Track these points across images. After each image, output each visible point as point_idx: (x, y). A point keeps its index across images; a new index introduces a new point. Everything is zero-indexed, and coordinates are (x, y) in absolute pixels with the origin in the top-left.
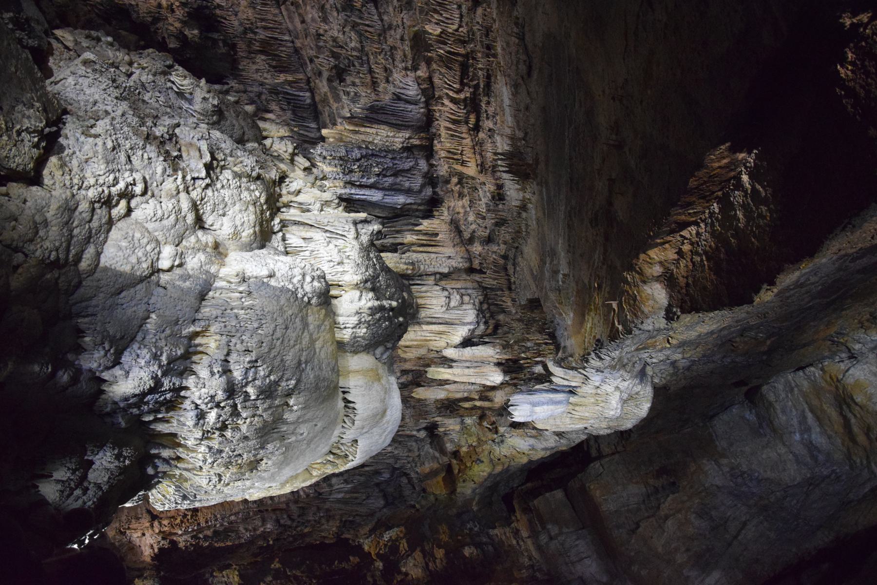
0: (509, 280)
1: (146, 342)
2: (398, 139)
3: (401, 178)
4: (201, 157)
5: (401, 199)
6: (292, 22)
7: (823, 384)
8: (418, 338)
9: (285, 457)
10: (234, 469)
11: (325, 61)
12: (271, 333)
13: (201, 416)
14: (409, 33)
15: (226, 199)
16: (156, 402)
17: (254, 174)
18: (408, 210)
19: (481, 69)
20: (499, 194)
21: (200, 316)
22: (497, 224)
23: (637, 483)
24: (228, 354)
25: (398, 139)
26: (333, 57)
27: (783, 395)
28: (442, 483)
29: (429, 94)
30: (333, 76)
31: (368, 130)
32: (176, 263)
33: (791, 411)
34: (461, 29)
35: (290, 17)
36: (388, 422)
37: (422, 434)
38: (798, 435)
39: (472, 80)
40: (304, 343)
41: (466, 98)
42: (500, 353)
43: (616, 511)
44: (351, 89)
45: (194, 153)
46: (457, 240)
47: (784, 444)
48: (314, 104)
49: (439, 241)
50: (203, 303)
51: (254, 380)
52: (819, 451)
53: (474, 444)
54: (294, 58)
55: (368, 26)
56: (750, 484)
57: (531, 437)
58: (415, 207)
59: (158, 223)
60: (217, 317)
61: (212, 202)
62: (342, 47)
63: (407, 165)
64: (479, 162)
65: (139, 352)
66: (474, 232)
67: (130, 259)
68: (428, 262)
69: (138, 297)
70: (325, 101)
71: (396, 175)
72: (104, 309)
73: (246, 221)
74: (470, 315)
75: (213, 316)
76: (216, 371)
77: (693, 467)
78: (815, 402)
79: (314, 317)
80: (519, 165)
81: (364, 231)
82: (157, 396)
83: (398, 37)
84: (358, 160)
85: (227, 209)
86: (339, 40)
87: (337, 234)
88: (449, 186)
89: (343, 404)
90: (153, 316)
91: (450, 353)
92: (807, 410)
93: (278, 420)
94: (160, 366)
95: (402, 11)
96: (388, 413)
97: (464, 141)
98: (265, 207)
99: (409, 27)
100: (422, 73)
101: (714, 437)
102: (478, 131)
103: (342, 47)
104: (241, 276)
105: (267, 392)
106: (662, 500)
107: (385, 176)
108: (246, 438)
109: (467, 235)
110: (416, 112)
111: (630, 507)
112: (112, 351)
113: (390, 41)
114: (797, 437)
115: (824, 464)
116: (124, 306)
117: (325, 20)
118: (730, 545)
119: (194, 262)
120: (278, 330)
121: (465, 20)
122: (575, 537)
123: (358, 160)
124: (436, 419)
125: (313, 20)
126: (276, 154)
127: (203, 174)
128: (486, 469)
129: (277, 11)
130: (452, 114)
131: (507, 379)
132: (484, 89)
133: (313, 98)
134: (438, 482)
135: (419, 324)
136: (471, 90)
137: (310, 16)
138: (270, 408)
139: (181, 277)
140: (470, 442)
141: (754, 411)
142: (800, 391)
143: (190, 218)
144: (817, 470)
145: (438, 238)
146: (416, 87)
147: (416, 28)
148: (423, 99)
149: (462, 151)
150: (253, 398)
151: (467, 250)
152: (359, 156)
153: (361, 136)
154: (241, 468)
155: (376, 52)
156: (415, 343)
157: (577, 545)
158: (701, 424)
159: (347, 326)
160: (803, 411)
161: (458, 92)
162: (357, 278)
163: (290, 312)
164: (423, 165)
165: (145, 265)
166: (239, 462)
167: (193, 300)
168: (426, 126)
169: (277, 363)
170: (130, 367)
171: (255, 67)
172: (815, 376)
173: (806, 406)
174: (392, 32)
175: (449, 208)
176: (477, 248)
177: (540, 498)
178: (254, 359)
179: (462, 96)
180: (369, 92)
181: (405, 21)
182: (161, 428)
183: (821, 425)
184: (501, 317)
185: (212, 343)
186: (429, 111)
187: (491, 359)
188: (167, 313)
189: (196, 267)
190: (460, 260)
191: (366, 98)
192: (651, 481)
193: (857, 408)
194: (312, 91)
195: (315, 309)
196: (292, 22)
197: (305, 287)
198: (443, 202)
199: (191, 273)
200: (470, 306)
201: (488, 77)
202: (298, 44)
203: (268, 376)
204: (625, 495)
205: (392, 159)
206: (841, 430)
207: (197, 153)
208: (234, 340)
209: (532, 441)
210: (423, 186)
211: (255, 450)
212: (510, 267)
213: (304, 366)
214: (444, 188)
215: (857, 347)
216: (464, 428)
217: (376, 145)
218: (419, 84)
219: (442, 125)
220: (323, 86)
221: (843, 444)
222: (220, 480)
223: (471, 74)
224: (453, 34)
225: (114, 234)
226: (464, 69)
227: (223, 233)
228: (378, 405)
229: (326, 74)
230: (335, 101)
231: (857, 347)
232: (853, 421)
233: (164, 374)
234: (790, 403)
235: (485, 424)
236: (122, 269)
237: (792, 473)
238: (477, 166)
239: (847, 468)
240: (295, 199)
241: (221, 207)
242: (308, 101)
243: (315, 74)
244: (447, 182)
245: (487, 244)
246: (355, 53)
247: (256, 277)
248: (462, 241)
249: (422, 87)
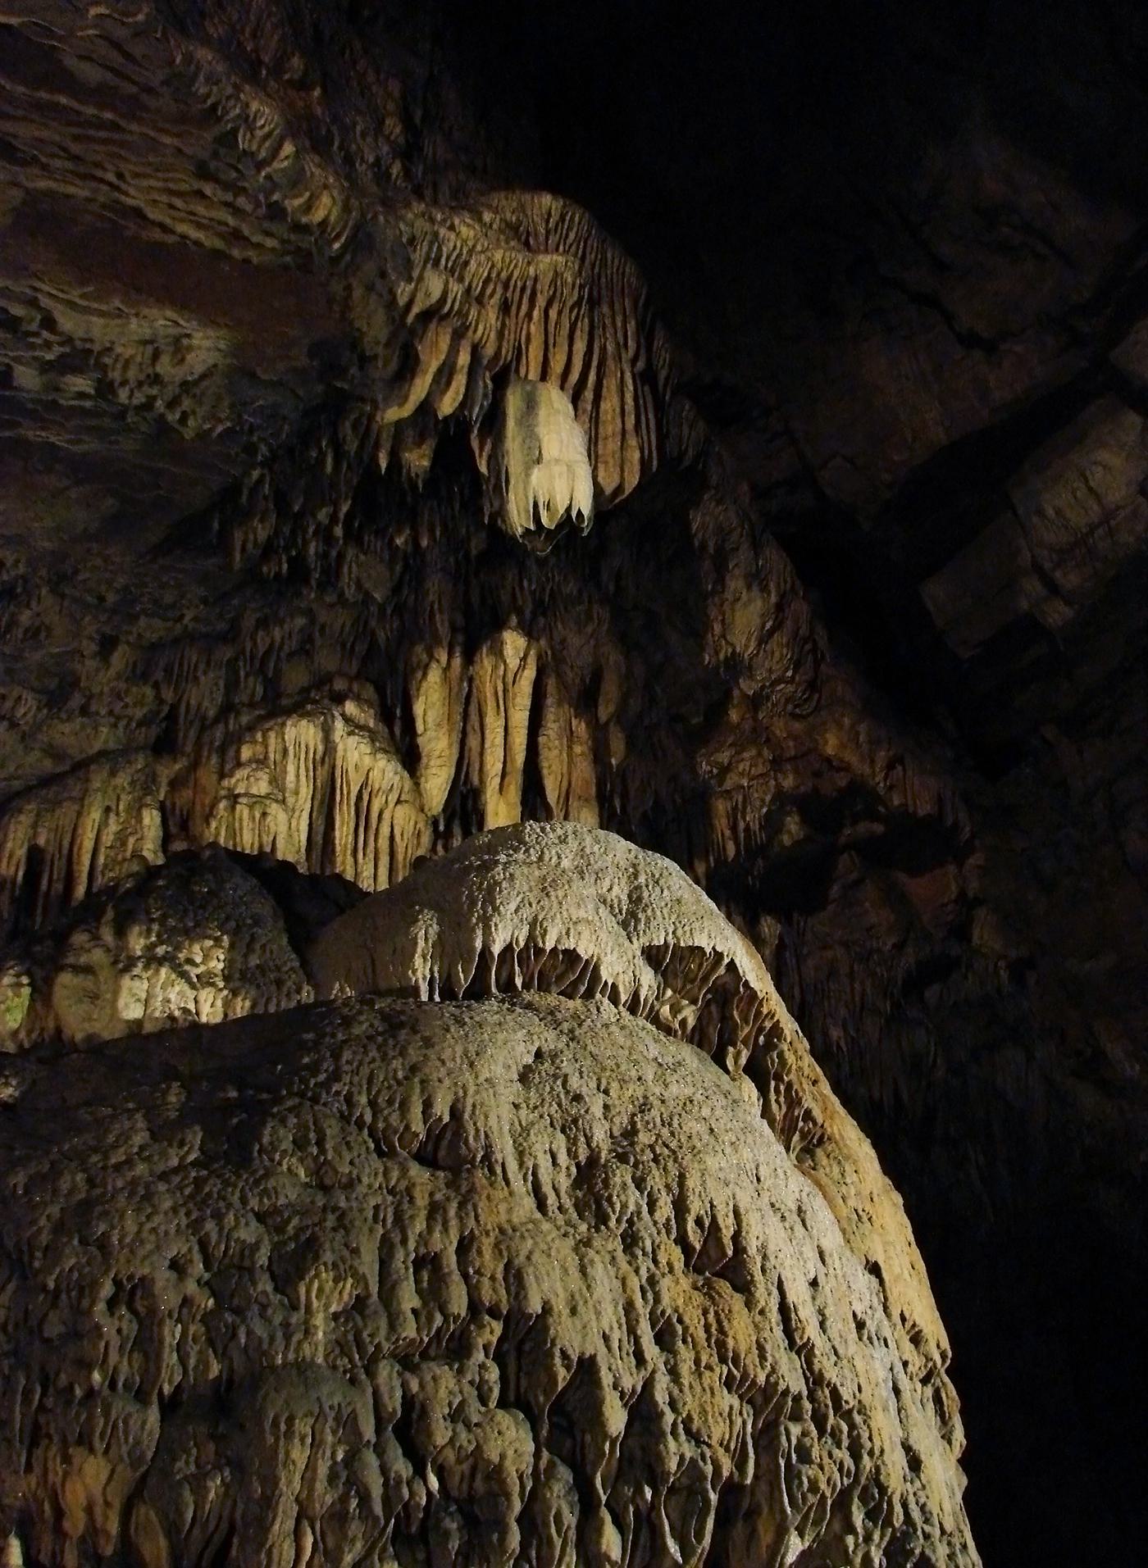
91: (437, 783)
131: (514, 620)
157: (1058, 512)
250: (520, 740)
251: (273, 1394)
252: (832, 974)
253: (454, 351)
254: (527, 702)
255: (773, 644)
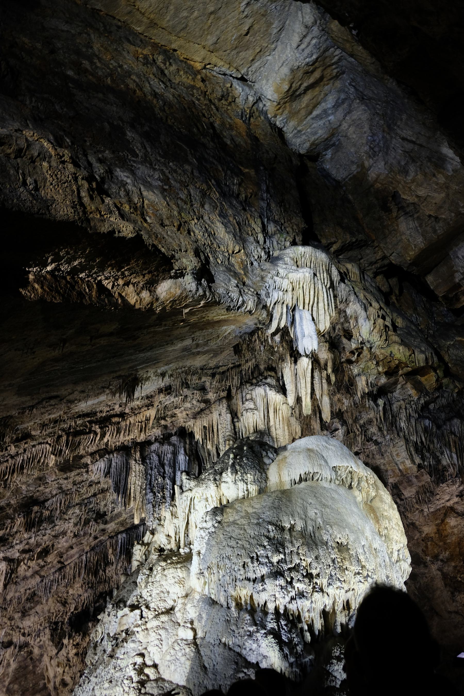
0: (232, 368)
1: (241, 644)
2: (137, 468)
3: (165, 461)
4: (126, 615)
5: (182, 458)
6: (74, 555)
7: (286, 112)
8: (281, 426)
9: (335, 524)
10: (347, 564)
11: (92, 528)
12: (232, 549)
13: (301, 595)
14: (61, 475)
15: (158, 592)
16: (290, 632)
17: (147, 572)
18: (191, 450)
19: (75, 423)
20: (166, 390)
21: (225, 604)
22: (188, 387)
23: (397, 225)
24: (249, 580)
25: (137, 468)
26: (89, 524)
27: (304, 137)
28: (426, 377)
29: (104, 452)
30: (103, 521)
31: (132, 491)
32: (189, 626)
33: (314, 128)
34: (49, 442)
35: (71, 557)
36: (318, 445)
37: (381, 402)
38: (330, 118)
39: (86, 426)
40: (244, 522)
41: (99, 428)
42: (287, 362)
43: (422, 235)
44: (110, 506)
45: (124, 620)
46: (207, 412)
47: (340, 125)
48: (127, 531)
49: (209, 425)
50: (218, 602)
51: (267, 557)
52: (339, 99)
53: (375, 363)
54: (98, 550)
55: (61, 503)
56: (377, 141)
57: (357, 322)
58: (187, 446)
59: (163, 643)
60: (225, 591)
61: (158, 603)
62: (80, 518)
63: (155, 458)
64: (146, 408)
65: (248, 649)
66: (198, 401)
67: (182, 662)
68: (224, 430)
69: (209, 653)
70: (122, 524)
71: (162, 465)
72: (215, 680)
73: (173, 575)
74: (259, 392)
75: (225, 593)
76: (261, 588)
77: (378, 185)
78: (303, 113)
79: (230, 516)
80: (130, 385)
81: (187, 486)
82: (283, 632)
83: (66, 481)
84: (155, 494)
85: (165, 591)
86: (75, 522)
87: (190, 504)
88: (169, 425)
89: (303, 483)
90: (223, 640)
91: (291, 399)
92: (311, 116)
93: (303, 534)
94: (258, 632)
95: (46, 483)
96: (310, 447)
97: (132, 422)
98: (169, 562)
99: (56, 475)
100: (88, 460)
101: (351, 176)
102: (125, 413)
103: (80, 518)
104: (199, 576)
105: (278, 546)
106: (408, 202)
107: (164, 472)
108: (317, 558)
109: (203, 405)
110: (116, 459)
111: (417, 225)
112: (246, 671)
113: (70, 486)
114: (331, 118)
115: (346, 92)
116: (215, 664)
117: (64, 533)
118: (421, 146)
119: (192, 613)
120: (231, 544)
121: (41, 440)
122: (457, 260)
123: (155, 494)
124: (359, 396)
125: (67, 541)
126: (144, 557)
127: (137, 612)
128: (396, 348)
129: (68, 567)
130: (113, 435)
132: (91, 417)
133: (122, 532)
134: (426, 380)
135: (269, 428)
136: (94, 425)
137: (65, 544)
138: (292, 542)
139: (199, 621)
140: (373, 366)
141: (324, 153)
142: (298, 125)
143: (164, 618)
144: (352, 97)
145: (207, 426)
146: (98, 463)
147: (57, 471)
148: (107, 456)
149: (139, 422)
150: (282, 556)
151: (214, 403)
152: (151, 494)
153: (137, 495)
154: (345, 558)
155: (79, 495)
156: (286, 428)
158: (344, 188)
159: (245, 489)
160: (313, 119)
161: (96, 434)
162: (212, 486)
163: (221, 536)
164: (154, 447)
165: (188, 650)
166: (339, 560)
167: (214, 610)
168: (125, 450)
169: (254, 542)
170: (260, 654)
171: (115, 576)
172: (283, 120)
173: (309, 118)
174: (63, 486)
175: (185, 422)
176: (211, 396)
177: (436, 293)
178: (250, 560)
179: (98, 430)
180: (109, 494)
181: (53, 479)
182: (318, 625)
183: (319, 103)
184: (262, 367)
185: (244, 592)
186: (116, 450)
187: (292, 369)
188: (221, 629)
189: (194, 610)
190: (221, 407)
191: (112, 496)
192: (395, 214)
193: (294, 85)
194: (117, 534)
195: (225, 516)
196: (74, 555)
197: (208, 527)
198: (181, 427)
199: (198, 614)
200: (253, 393)
201: (79, 416)
202: (87, 549)
203: (265, 547)
204: (409, 232)
205: (152, 470)
206: (317, 89)
207: (124, 618)
208: (239, 577)
209: (361, 321)
210: (170, 444)
211: (328, 549)
212: (221, 370)
213: (261, 520)
214: (171, 428)
215: (251, 99)
216: (362, 372)
217: (142, 483)
218: (97, 461)
219: (125, 439)
220: (111, 527)
221: (328, 84)
222: (359, 573)
223: (82, 428)
224: (53, 447)
225: (166, 676)
226: (77, 433)
227: (179, 592)
228: (301, 456)
229: (102, 526)
230: (121, 516)
231: (251, 99)
232: (305, 85)
233: (264, 627)
234: (309, 130)
235: (353, 359)
236: (188, 668)
237: (360, 113)
238: (148, 409)
239: (345, 75)
240: (174, 538)
241: (162, 595)
242: (124, 535)
243: (104, 534)
244: (166, 427)
245: (206, 390)
246: (83, 509)
247: (199, 564)
248: (208, 408)
249: (98, 458)
250: (309, 385)
251: (196, 264)
252: (400, 407)
253: (282, 308)
254: (310, 375)
255: (374, 333)
